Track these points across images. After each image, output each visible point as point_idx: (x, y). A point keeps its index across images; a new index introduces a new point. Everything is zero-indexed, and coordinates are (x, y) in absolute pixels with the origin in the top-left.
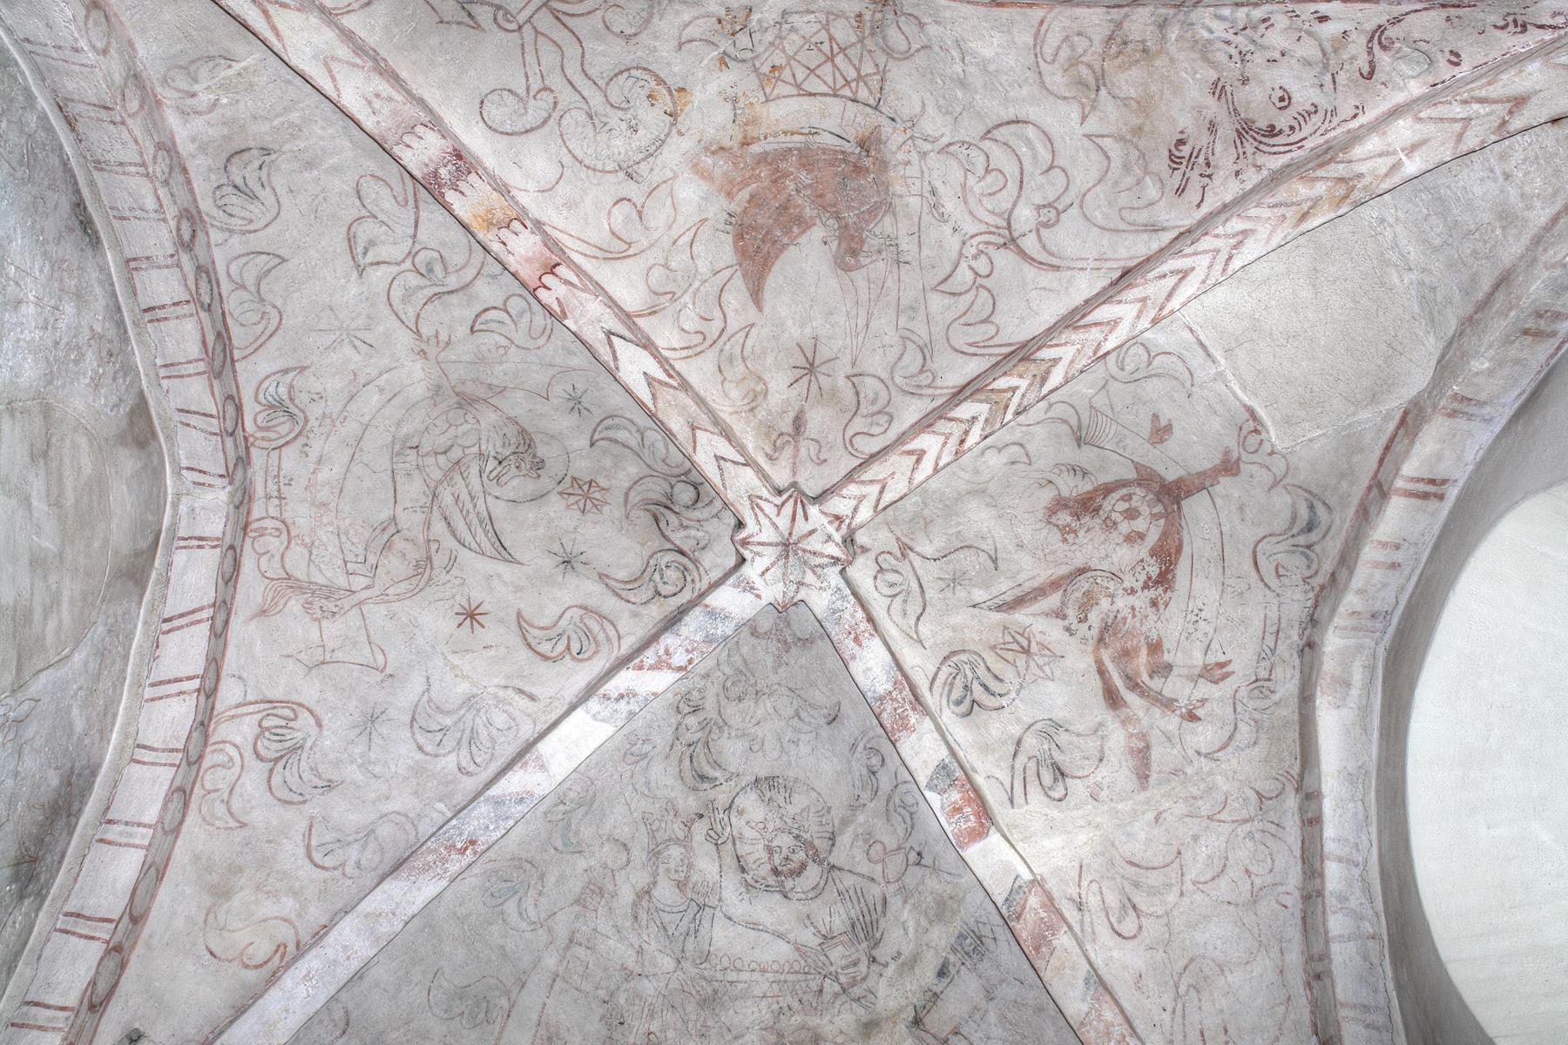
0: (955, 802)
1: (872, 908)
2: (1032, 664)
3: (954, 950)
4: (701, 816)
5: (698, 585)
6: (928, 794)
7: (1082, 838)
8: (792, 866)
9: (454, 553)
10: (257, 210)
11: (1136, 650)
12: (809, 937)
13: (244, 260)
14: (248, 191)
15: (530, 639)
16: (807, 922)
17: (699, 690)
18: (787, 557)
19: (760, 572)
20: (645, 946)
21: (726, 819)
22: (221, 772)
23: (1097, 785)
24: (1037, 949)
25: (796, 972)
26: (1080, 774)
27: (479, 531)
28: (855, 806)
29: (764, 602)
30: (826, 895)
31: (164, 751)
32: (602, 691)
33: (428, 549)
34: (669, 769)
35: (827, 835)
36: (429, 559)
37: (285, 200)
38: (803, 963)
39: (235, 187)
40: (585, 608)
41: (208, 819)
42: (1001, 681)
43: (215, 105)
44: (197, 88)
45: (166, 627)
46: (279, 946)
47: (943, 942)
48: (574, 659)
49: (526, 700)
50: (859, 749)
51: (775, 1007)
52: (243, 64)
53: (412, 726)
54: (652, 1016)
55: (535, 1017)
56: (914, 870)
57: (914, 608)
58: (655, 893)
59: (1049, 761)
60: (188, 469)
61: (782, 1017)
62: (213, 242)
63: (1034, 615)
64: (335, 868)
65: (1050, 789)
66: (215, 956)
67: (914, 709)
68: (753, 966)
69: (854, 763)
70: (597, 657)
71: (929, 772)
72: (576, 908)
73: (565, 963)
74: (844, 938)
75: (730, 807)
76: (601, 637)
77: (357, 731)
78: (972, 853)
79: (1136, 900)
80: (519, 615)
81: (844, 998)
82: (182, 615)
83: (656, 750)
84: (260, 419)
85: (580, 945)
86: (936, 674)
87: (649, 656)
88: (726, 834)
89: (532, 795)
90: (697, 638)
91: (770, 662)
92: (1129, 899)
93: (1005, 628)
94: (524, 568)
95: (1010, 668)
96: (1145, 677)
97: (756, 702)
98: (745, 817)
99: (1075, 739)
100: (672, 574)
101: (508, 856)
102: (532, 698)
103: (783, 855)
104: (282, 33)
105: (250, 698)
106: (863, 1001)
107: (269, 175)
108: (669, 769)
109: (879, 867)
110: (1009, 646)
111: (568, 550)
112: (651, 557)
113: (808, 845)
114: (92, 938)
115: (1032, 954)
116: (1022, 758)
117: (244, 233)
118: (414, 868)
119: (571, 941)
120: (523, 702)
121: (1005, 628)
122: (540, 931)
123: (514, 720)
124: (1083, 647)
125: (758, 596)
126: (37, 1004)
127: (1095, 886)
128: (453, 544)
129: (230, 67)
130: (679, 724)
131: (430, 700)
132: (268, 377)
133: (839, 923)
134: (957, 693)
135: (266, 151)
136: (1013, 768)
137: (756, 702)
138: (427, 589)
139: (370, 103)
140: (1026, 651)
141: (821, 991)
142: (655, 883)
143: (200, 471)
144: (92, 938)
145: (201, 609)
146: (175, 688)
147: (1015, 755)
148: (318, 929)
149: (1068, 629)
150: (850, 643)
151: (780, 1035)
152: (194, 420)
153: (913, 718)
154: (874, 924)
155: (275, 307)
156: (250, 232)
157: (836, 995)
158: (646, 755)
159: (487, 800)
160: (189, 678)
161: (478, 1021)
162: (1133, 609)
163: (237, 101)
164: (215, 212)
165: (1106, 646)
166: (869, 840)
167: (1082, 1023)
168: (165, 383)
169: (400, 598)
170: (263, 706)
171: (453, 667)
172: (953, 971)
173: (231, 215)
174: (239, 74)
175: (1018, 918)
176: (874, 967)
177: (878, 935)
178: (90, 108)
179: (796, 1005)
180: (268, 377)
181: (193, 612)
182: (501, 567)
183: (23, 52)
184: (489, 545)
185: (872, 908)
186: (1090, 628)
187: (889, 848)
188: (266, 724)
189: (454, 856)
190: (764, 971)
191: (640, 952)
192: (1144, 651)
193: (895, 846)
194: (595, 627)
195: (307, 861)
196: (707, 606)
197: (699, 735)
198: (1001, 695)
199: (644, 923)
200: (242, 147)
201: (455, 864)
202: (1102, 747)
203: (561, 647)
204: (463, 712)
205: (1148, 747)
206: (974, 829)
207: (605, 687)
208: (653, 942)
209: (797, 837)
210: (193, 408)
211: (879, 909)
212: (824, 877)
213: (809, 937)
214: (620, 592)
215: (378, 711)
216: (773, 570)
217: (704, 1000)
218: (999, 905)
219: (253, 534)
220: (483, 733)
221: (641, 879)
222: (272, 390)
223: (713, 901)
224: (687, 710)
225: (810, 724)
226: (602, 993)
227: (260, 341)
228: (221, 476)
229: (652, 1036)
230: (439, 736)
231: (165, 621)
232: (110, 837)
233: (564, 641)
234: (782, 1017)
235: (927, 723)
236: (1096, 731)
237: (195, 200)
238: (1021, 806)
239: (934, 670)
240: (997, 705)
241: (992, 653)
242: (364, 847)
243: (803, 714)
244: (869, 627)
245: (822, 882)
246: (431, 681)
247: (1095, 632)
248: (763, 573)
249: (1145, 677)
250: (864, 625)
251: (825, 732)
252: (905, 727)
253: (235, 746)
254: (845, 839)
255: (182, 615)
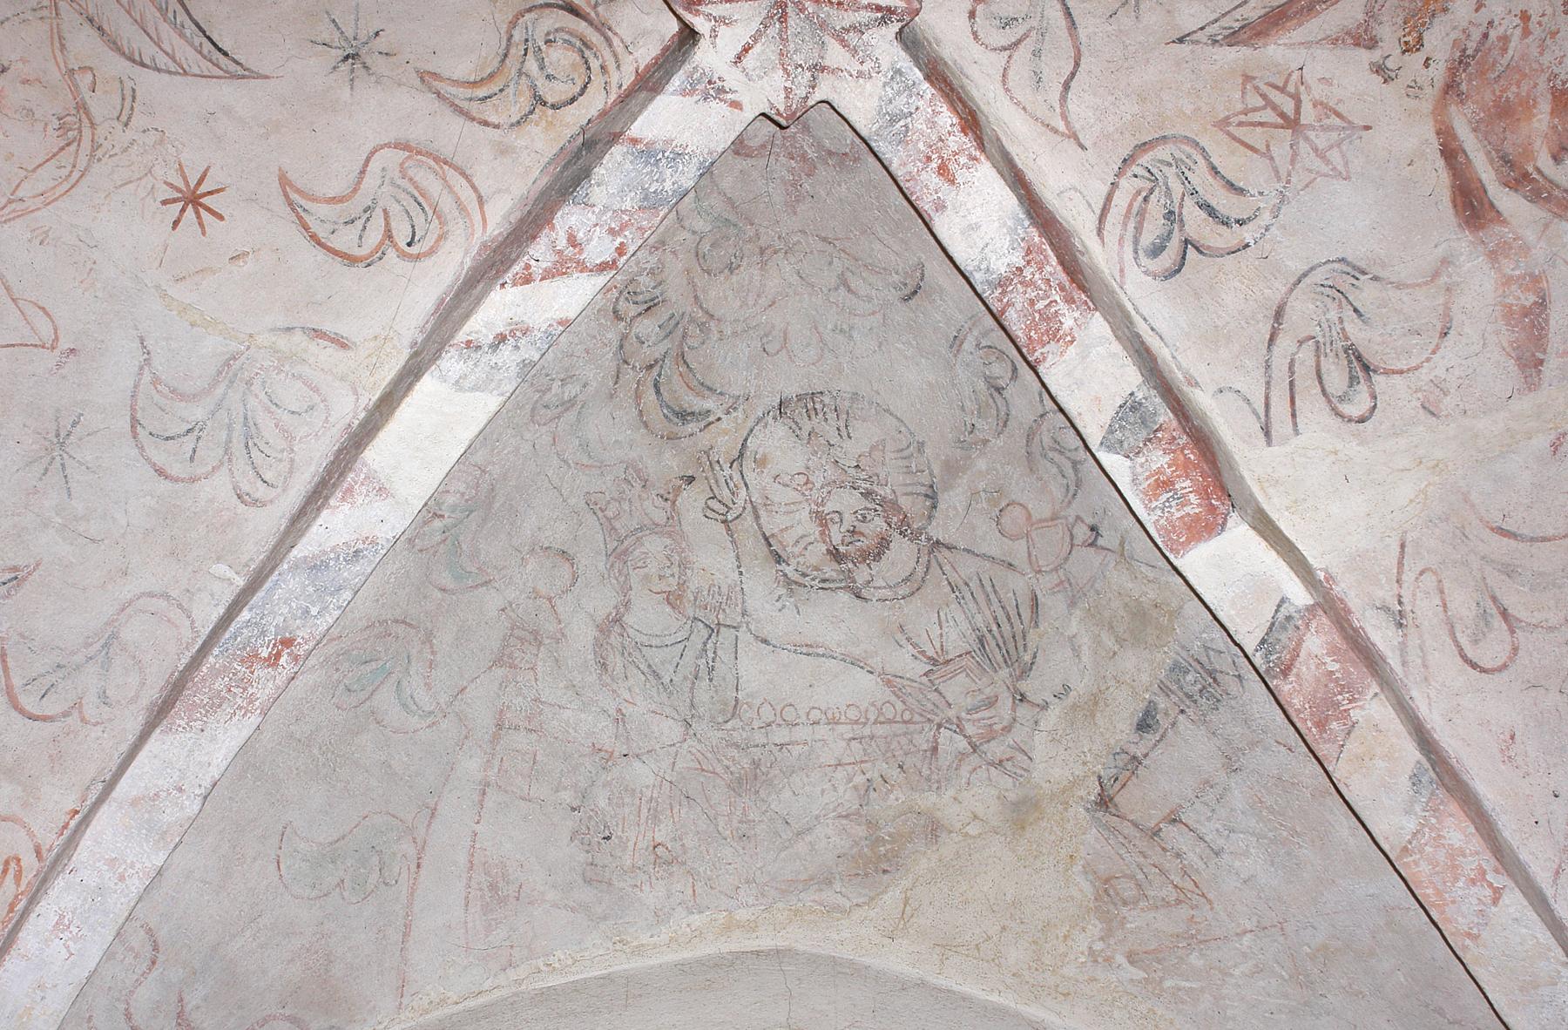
0: (1159, 471)
1: (1013, 613)
2: (1304, 147)
3: (1164, 689)
4: (691, 480)
5: (615, 78)
6: (1102, 456)
7: (1405, 491)
8: (864, 543)
9: (128, 84)
11: (1528, 104)
12: (908, 665)
15: (315, 227)
16: (899, 636)
17: (652, 272)
18: (783, 18)
19: (732, 56)
20: (628, 710)
21: (737, 477)
23: (1436, 384)
24: (1321, 725)
25: (890, 722)
26: (1402, 365)
27: (166, 30)
28: (969, 442)
29: (749, 113)
30: (928, 589)
32: (461, 336)
33: (75, 89)
34: (617, 414)
35: (923, 490)
36: (82, 107)
38: (900, 706)
40: (406, 147)
42: (1241, 191)
46: (7, 863)
47: (1145, 678)
48: (403, 255)
49: (332, 350)
50: (968, 345)
51: (860, 779)
53: (135, 435)
54: (655, 818)
55: (462, 859)
56: (1082, 553)
57: (1056, 66)
58: (629, 619)
59: (1339, 345)
61: (873, 795)
63: (1307, 44)
64: (66, 714)
65: (1341, 399)
67: (1070, 300)
68: (815, 715)
69: (959, 370)
70: (447, 246)
71: (1106, 417)
72: (499, 672)
73: (496, 763)
74: (967, 661)
75: (741, 455)
76: (447, 204)
77: (38, 468)
78: (1196, 561)
79: (1509, 601)
80: (284, 181)
81: (974, 760)
83: (590, 389)
85: (517, 728)
86: (1109, 198)
87: (540, 253)
88: (740, 502)
89: (374, 543)
90: (628, 205)
91: (779, 197)
92: (1494, 599)
93: (1248, 78)
94: (272, 82)
95: (1260, 163)
96: (1544, 161)
97: (763, 265)
98: (771, 469)
99: (1392, 293)
100: (561, 58)
101: (364, 623)
102: (342, 343)
103: (846, 526)
106: (1008, 765)
108: (617, 414)
109: (1021, 546)
110: (1256, 117)
111: (350, 33)
112: (513, 24)
113: (889, 506)
115: (1312, 733)
116: (1285, 344)
118: (194, 704)
119: (499, 726)
120: (325, 354)
121: (1248, 78)
122: (444, 725)
123: (316, 390)
124: (1412, 103)
125: (736, 105)
127: (1429, 581)
128: (118, 66)
130: (624, 337)
131: (156, 381)
133: (956, 636)
134: (1153, 228)
136: (1268, 367)
137: (763, 265)
138: (96, 167)
140: (1292, 123)
141: (935, 749)
142: (627, 605)
147: (1272, 340)
148: (64, 818)
149: (1379, 69)
150: (931, 179)
151: (872, 825)
153: (1068, 318)
154: (1019, 639)
157: (962, 756)
158: (572, 402)
159: (295, 567)
161: (370, 887)
162: (1525, 17)
165: (1462, 98)
166: (1000, 505)
167: (1405, 849)
169: (47, 198)
171: (184, 309)
172: (1164, 723)
175: (1285, 673)
176: (1023, 711)
177: (1027, 658)
179: (894, 773)
182: (227, 92)
184: (192, 54)
185: (1013, 613)
186: (1426, 64)
187: (1036, 516)
189: (261, 672)
190: (834, 722)
191: (620, 718)
192: (1545, 106)
193: (1047, 514)
194: (434, 186)
195: (14, 714)
196: (635, 141)
197: (666, 345)
198: (1241, 222)
199: (619, 669)
201: (265, 684)
202: (1447, 308)
203: (374, 236)
204: (220, 390)
205: (1542, 304)
206: (1197, 518)
207: (466, 328)
208: (639, 700)
209: (867, 494)
211: (1026, 614)
212: (924, 559)
213: (908, 665)
214: (465, 105)
215: (66, 423)
216: (758, 48)
217: (739, 780)
218: (1249, 652)
220: (266, 425)
221: (602, 602)
223: (733, 616)
224: (633, 310)
225: (869, 299)
226: (567, 797)
229: (660, 850)
230: (188, 443)
233: (378, 222)
234: (873, 795)
235: (1098, 325)
236: (1436, 275)
238: (1285, 441)
239: (1105, 189)
240: (1234, 243)
241: (1221, 136)
242: (107, 665)
243: (855, 283)
244: (967, 142)
245: (920, 570)
246: (149, 343)
247: (1438, 72)
248: (739, 58)
249: (1544, 161)
250: (959, 141)
251: (900, 314)
252: (1054, 335)
254: (953, 499)
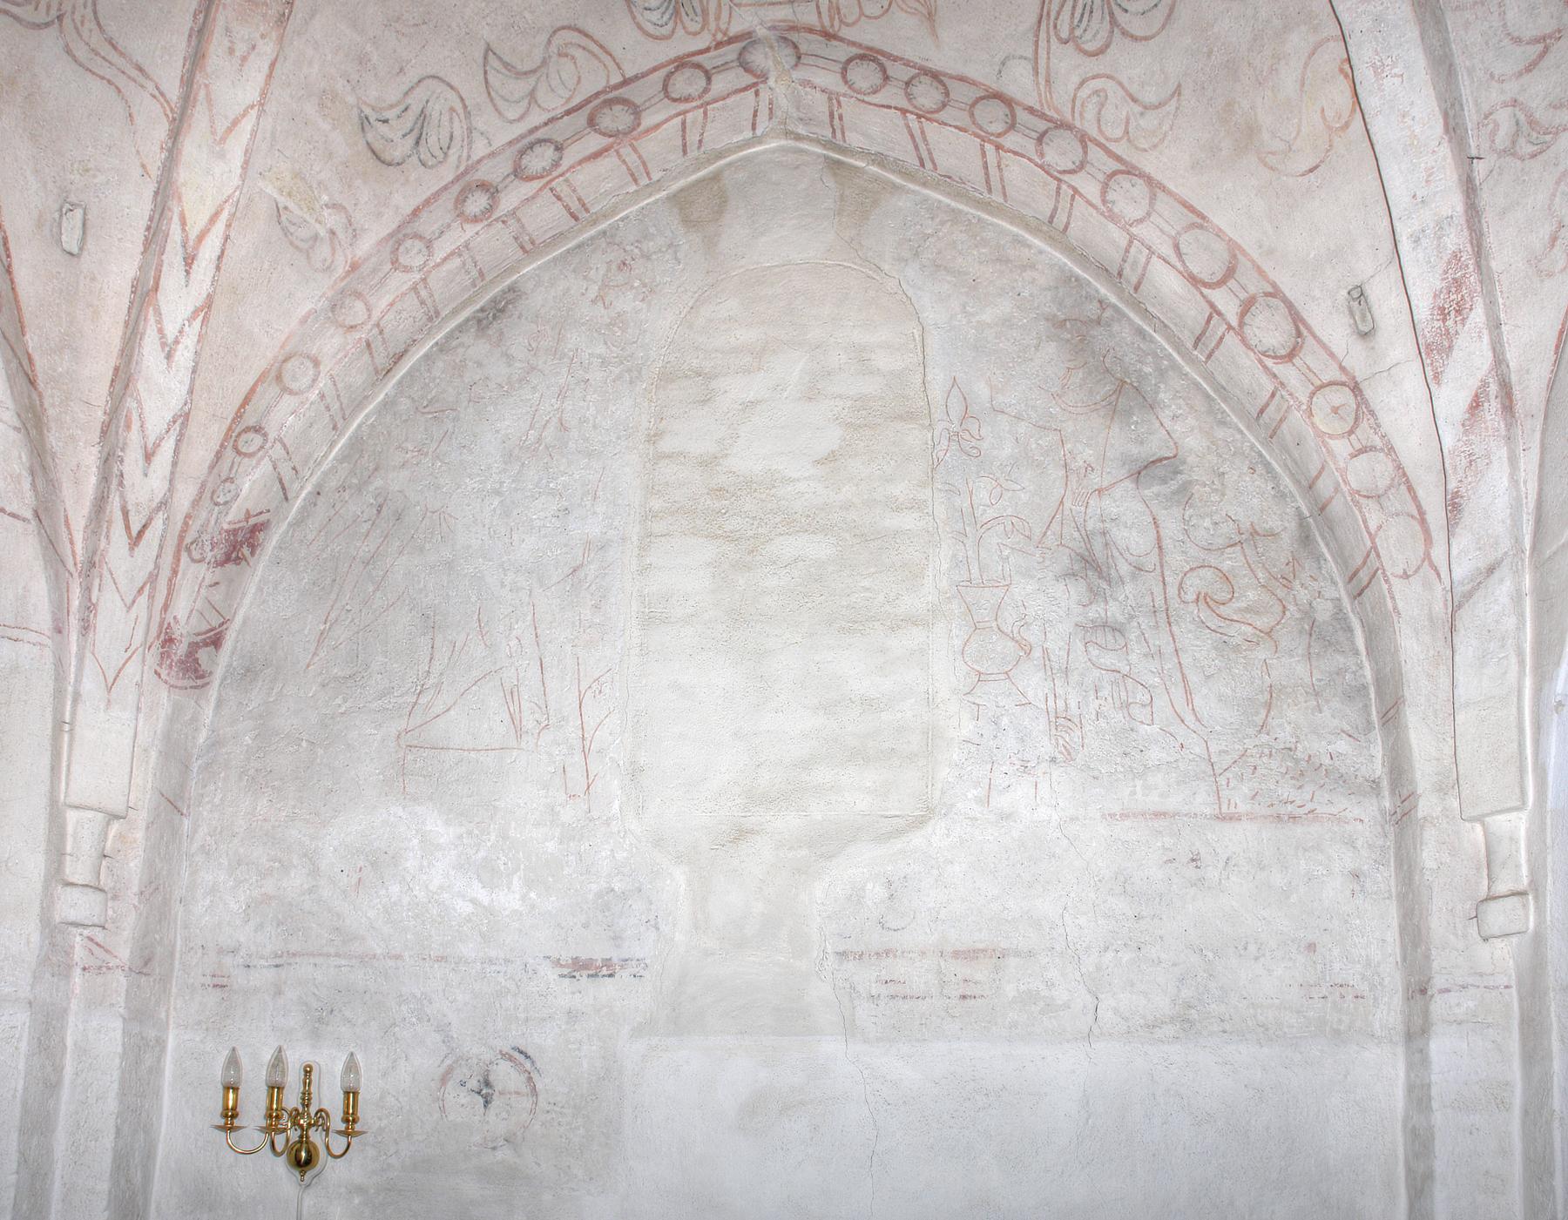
10: (437, 107)
13: (499, 102)
14: (419, 125)
22: (1109, 113)
31: (1057, 201)
37: (413, 75)
39: (417, 143)
41: (1156, 140)
43: (334, 206)
44: (322, 233)
45: (929, 165)
52: (276, 195)
60: (754, 127)
62: (488, 151)
66: (1316, 167)
82: (916, 147)
84: (695, 27)
104: (213, 211)
105: (1029, 53)
107: (391, 106)
114: (1221, 339)
117: (468, 114)
126: (1262, 411)
129: (286, 208)
132: (640, 27)
135: (364, 122)
139: (244, 59)
143: (755, 115)
144: (1221, 339)
145: (908, 127)
146: (993, 171)
152: (693, 138)
155: (549, 42)
156: (465, 107)
160: (984, 154)
163: (320, 183)
164: (453, 159)
168: (655, 177)
170: (1043, 35)
173: (451, 137)
174: (290, 194)
178: (375, 355)
180: (640, 27)
181: (912, 136)
183: (346, 428)
188: (1064, 34)
200: (370, 154)
210: (680, 142)
219: (836, 23)
222: (654, 16)
227: (596, 49)
228: (757, 94)
231: (923, 165)
232: (1134, 280)
237: (445, 188)
253: (1082, 83)
255: (916, 147)
